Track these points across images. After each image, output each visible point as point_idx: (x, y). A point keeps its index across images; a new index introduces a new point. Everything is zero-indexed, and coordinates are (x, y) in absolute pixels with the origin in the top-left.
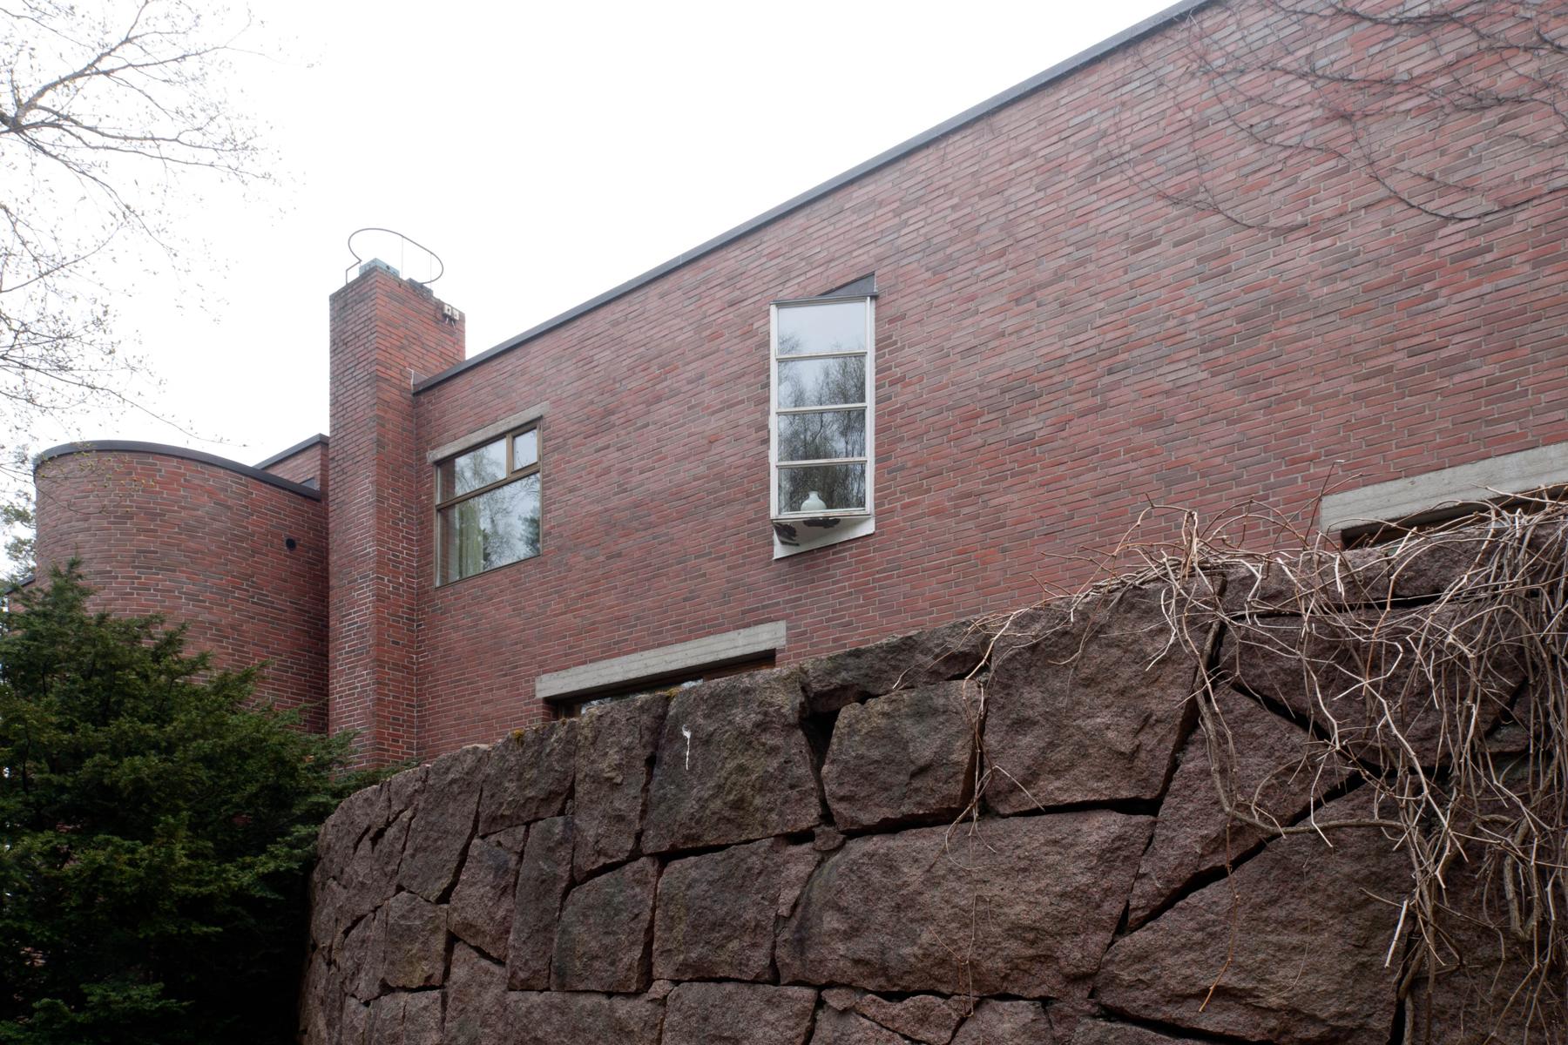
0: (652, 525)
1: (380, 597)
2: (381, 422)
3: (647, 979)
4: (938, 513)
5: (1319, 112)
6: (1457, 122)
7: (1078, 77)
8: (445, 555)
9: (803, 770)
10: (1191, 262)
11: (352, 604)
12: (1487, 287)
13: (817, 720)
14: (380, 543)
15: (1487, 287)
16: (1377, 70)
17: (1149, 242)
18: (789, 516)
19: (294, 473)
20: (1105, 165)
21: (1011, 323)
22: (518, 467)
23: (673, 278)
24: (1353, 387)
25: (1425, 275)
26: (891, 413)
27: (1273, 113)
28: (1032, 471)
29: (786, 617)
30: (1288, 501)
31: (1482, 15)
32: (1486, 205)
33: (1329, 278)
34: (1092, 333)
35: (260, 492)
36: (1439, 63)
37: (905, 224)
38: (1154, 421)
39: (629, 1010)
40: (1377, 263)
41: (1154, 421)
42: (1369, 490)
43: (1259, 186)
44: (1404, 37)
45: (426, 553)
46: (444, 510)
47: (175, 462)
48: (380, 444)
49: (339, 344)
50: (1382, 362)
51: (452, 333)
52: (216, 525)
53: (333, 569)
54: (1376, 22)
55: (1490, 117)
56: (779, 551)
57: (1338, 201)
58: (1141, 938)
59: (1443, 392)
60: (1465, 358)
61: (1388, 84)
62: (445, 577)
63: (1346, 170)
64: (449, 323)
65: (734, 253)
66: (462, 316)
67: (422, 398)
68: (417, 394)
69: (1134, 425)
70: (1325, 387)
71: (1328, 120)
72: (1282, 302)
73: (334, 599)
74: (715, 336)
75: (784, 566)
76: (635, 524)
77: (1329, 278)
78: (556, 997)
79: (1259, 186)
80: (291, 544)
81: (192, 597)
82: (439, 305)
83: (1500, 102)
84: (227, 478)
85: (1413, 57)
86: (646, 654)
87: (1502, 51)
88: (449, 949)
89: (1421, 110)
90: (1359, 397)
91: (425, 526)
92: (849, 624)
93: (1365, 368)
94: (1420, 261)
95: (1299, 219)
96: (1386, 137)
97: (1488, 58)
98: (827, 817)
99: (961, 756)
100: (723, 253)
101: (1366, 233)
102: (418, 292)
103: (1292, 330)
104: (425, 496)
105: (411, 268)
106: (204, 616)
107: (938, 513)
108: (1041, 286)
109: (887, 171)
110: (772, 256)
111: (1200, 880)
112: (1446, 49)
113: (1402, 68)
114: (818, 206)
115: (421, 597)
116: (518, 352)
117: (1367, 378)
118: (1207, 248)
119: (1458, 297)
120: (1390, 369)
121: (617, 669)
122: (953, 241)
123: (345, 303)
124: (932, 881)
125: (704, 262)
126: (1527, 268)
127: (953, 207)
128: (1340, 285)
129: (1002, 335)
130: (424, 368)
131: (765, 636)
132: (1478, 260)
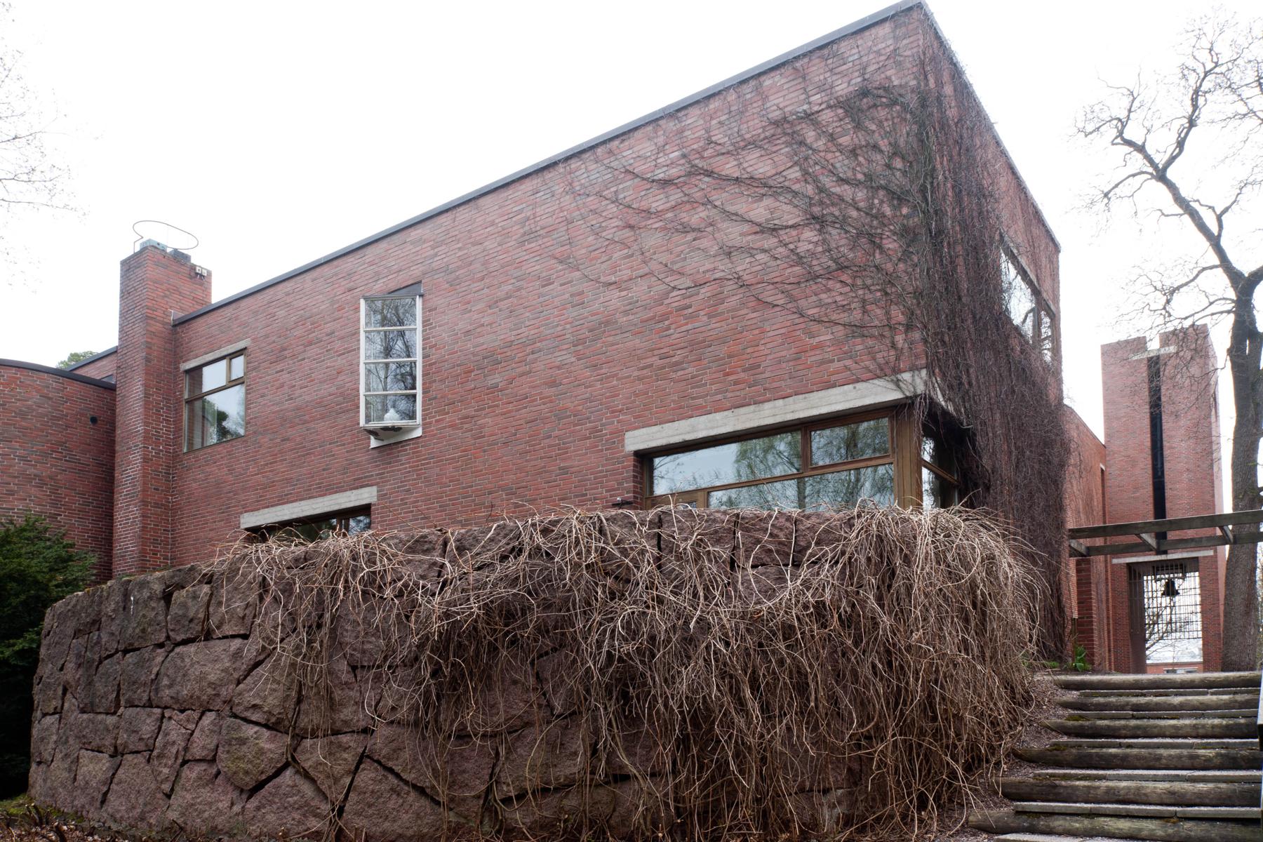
0: (305, 422)
1: (146, 460)
2: (149, 346)
3: (118, 706)
4: (453, 426)
5: (620, 223)
6: (677, 238)
7: (517, 184)
8: (191, 430)
9: (161, 618)
10: (567, 296)
11: (129, 463)
12: (690, 327)
13: (167, 597)
14: (146, 424)
15: (690, 327)
16: (644, 205)
17: (548, 282)
18: (374, 425)
19: (92, 372)
20: (529, 236)
21: (486, 320)
22: (234, 378)
23: (318, 270)
24: (636, 373)
25: (665, 317)
26: (431, 365)
27: (601, 219)
28: (497, 406)
29: (377, 484)
30: (611, 433)
31: (685, 183)
32: (689, 284)
33: (626, 313)
34: (524, 329)
35: (72, 388)
36: (668, 205)
37: (436, 255)
38: (553, 383)
39: (111, 720)
40: (645, 307)
41: (553, 383)
42: (644, 430)
43: (596, 258)
44: (655, 189)
45: (178, 429)
46: (189, 402)
47: (13, 371)
48: (148, 360)
49: (125, 293)
50: (649, 361)
51: (202, 285)
52: (40, 410)
53: (118, 439)
54: (644, 179)
55: (690, 237)
56: (374, 443)
57: (629, 272)
58: (241, 686)
59: (672, 380)
60: (682, 363)
61: (648, 212)
62: (191, 444)
63: (632, 255)
64: (200, 279)
65: (350, 259)
66: (209, 273)
67: (179, 329)
68: (175, 326)
69: (545, 383)
70: (626, 372)
71: (625, 227)
72: (607, 323)
73: (118, 460)
74: (340, 309)
75: (376, 453)
76: (297, 420)
77: (626, 313)
78: (91, 716)
79: (596, 258)
80: (94, 420)
81: (23, 458)
82: (193, 267)
83: (694, 230)
84: (50, 380)
85: (658, 201)
86: (303, 503)
87: (693, 203)
88: (64, 694)
89: (664, 229)
90: (640, 379)
91: (178, 412)
92: (409, 490)
93: (643, 363)
94: (661, 310)
95: (613, 279)
96: (652, 240)
97: (688, 206)
98: (168, 638)
99: (201, 615)
100: (344, 259)
101: (640, 290)
102: (179, 258)
103: (611, 339)
104: (178, 390)
105: (172, 241)
106: (31, 471)
107: (453, 426)
108: (501, 300)
109: (428, 223)
110: (371, 264)
111: (257, 664)
112: (671, 198)
113: (654, 205)
114: (395, 237)
115: (175, 457)
116: (234, 306)
117: (643, 369)
118: (573, 290)
119: (679, 330)
120: (651, 365)
121: (286, 512)
122: (459, 268)
123: (130, 267)
124: (192, 665)
125: (335, 263)
126: (705, 318)
127: (460, 249)
128: (631, 317)
129: (483, 325)
130: (181, 308)
131: (366, 495)
132: (686, 312)
